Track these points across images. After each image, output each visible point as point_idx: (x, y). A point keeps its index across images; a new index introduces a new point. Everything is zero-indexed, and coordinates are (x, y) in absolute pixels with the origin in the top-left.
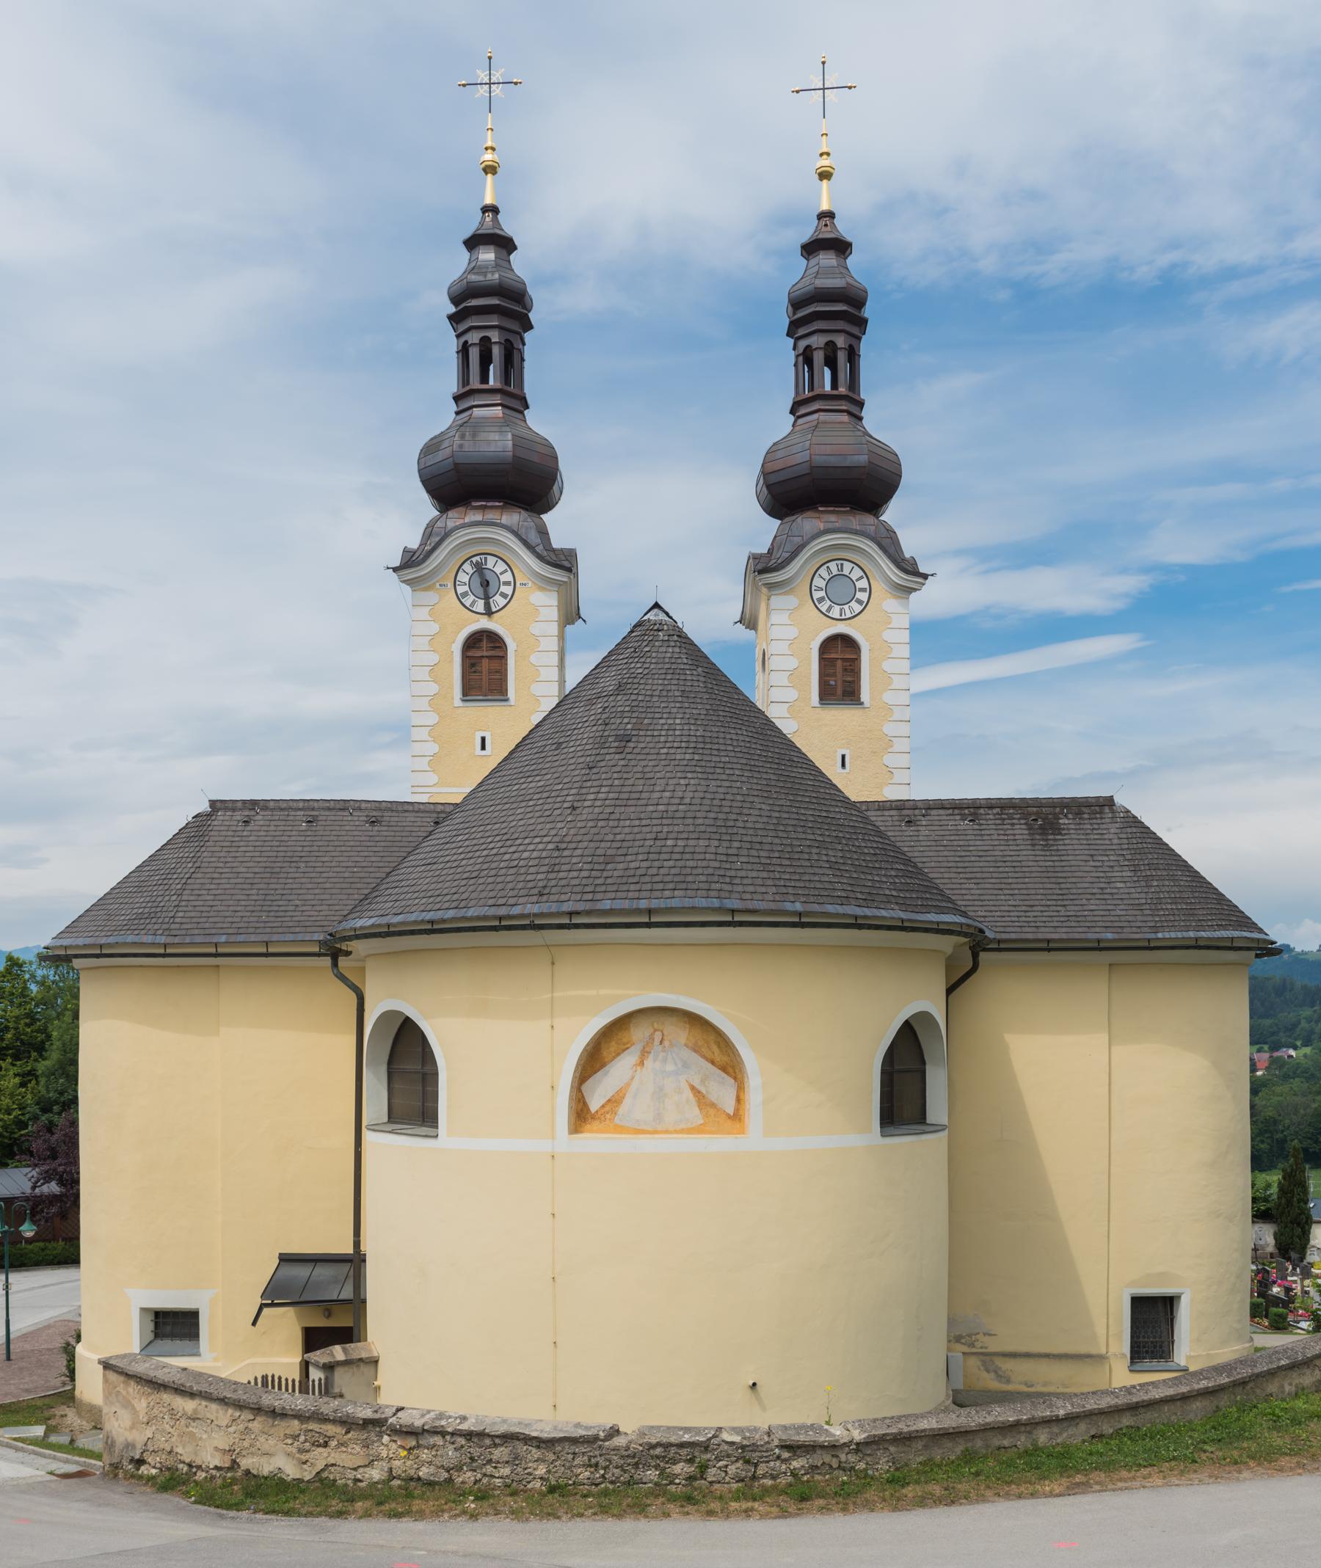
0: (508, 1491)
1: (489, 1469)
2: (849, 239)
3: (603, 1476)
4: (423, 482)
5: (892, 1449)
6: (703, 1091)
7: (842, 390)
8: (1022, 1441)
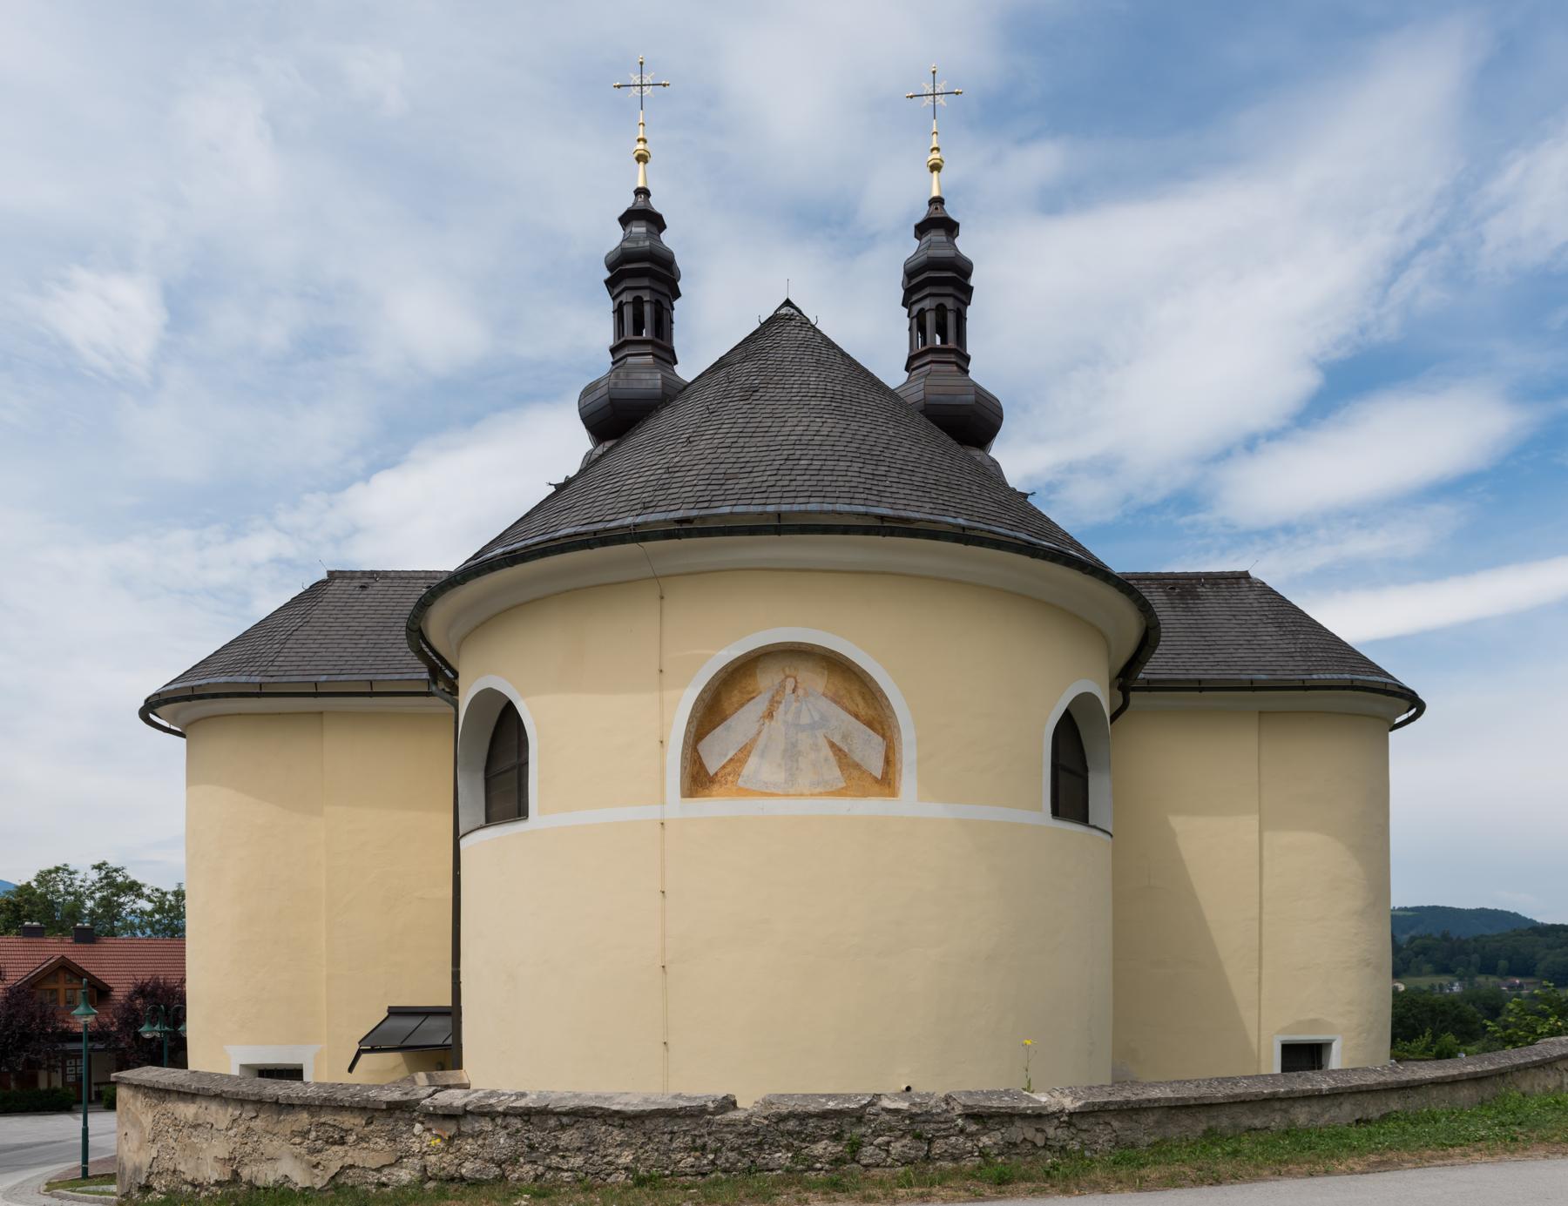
0: (578, 1186)
1: (555, 1160)
2: (956, 219)
3: (713, 1162)
4: (583, 420)
5: (1116, 1124)
6: (846, 749)
7: (951, 344)
8: (1277, 1121)
